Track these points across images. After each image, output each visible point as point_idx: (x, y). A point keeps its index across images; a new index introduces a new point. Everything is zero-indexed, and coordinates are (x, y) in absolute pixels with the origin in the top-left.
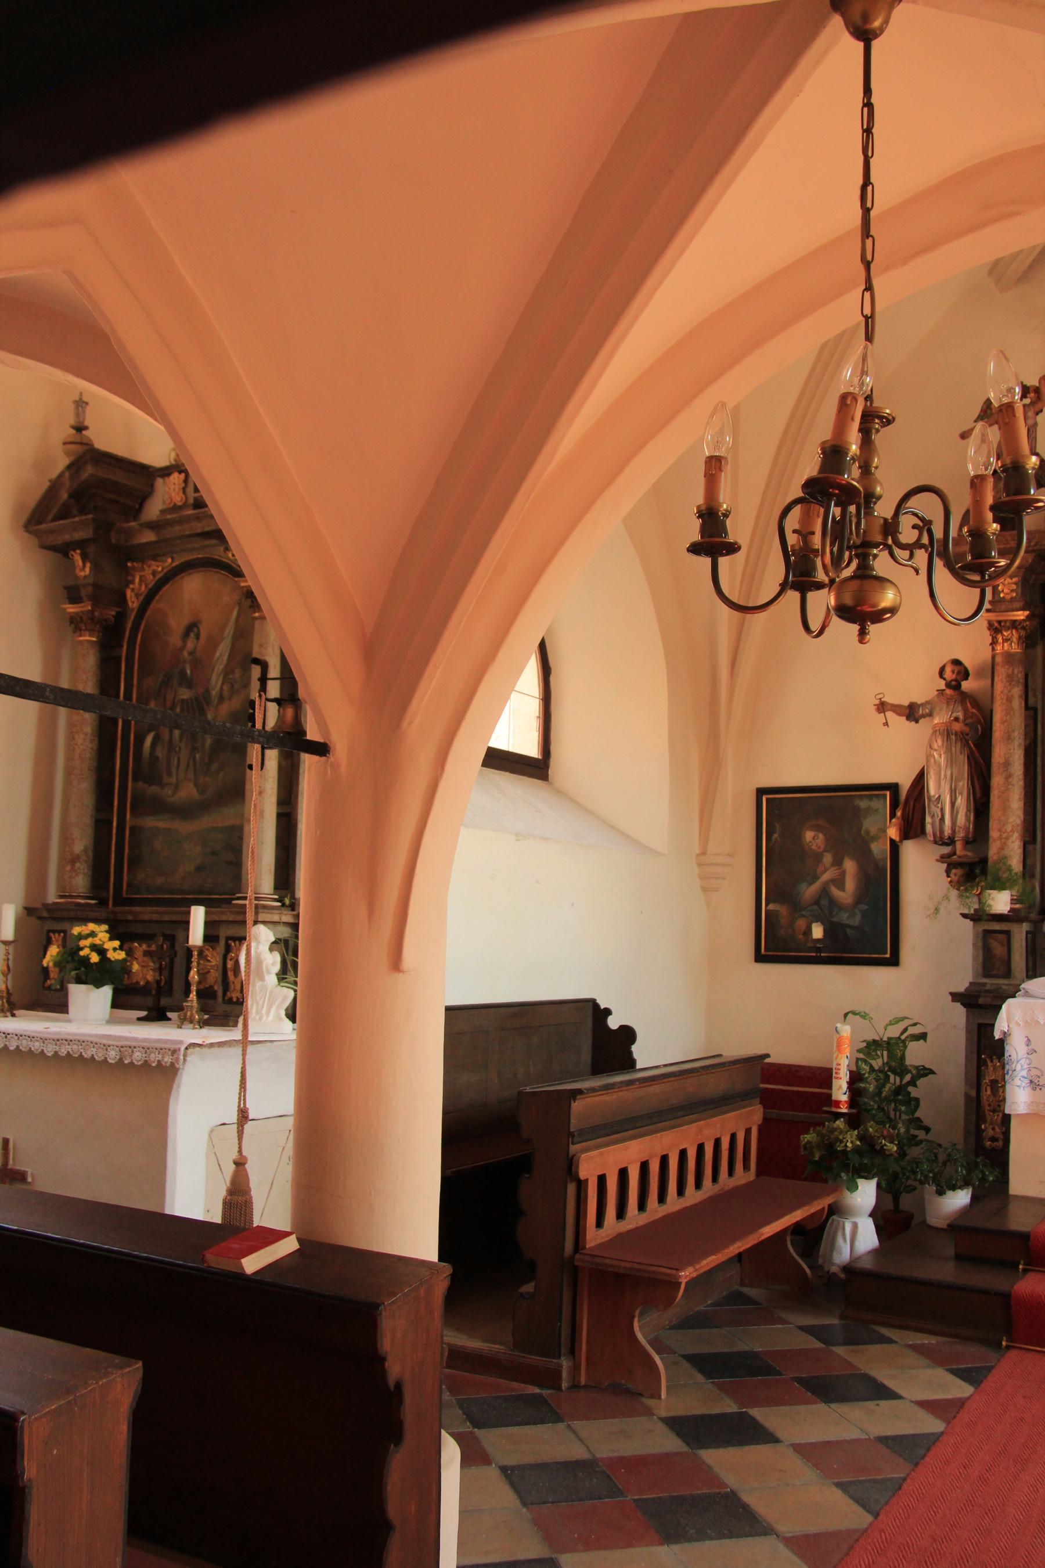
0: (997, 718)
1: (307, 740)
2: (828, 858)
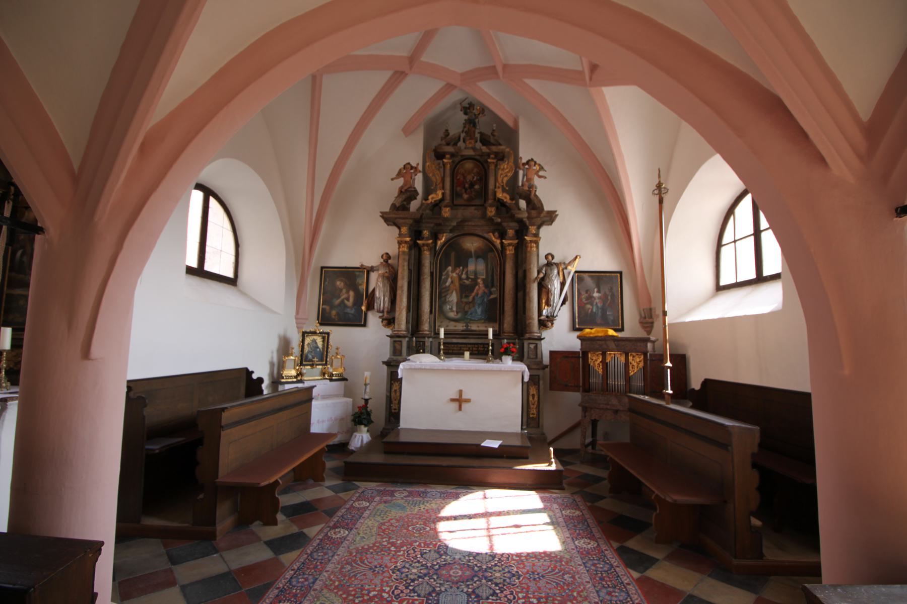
0: (400, 272)
2: (344, 291)
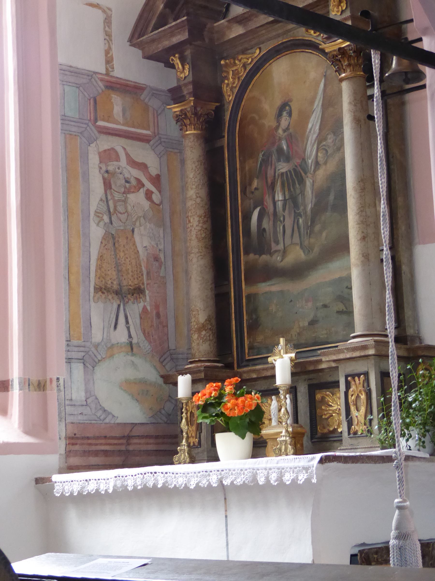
1: (423, 51)
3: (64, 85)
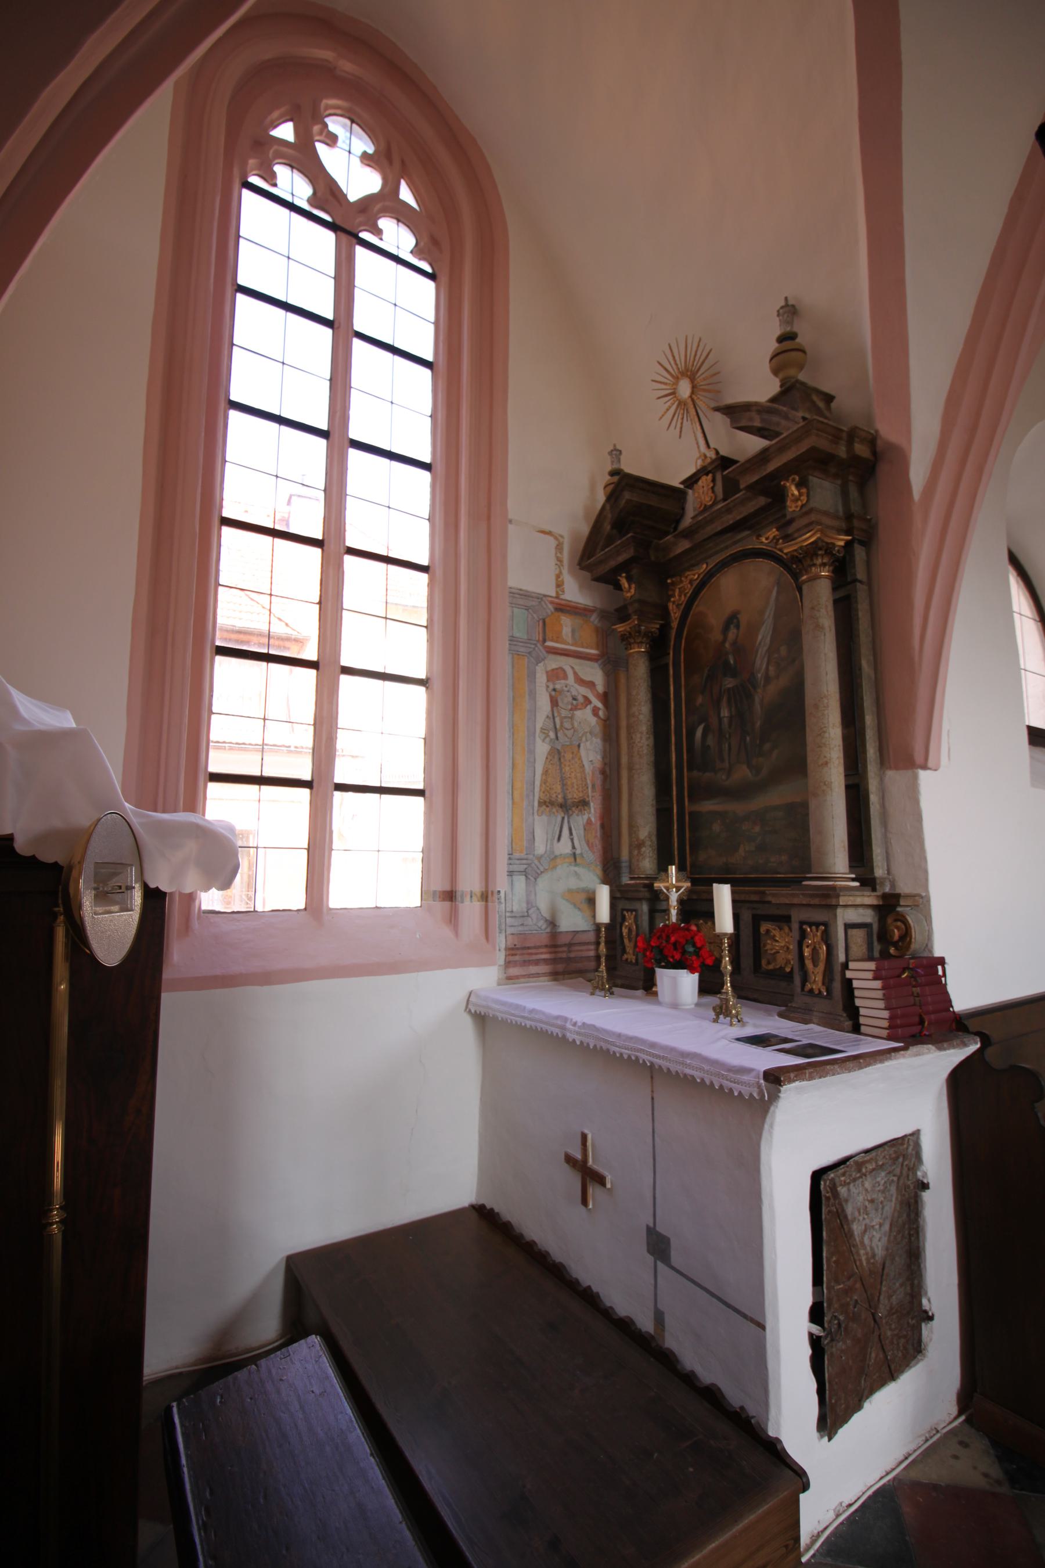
3: (513, 607)
